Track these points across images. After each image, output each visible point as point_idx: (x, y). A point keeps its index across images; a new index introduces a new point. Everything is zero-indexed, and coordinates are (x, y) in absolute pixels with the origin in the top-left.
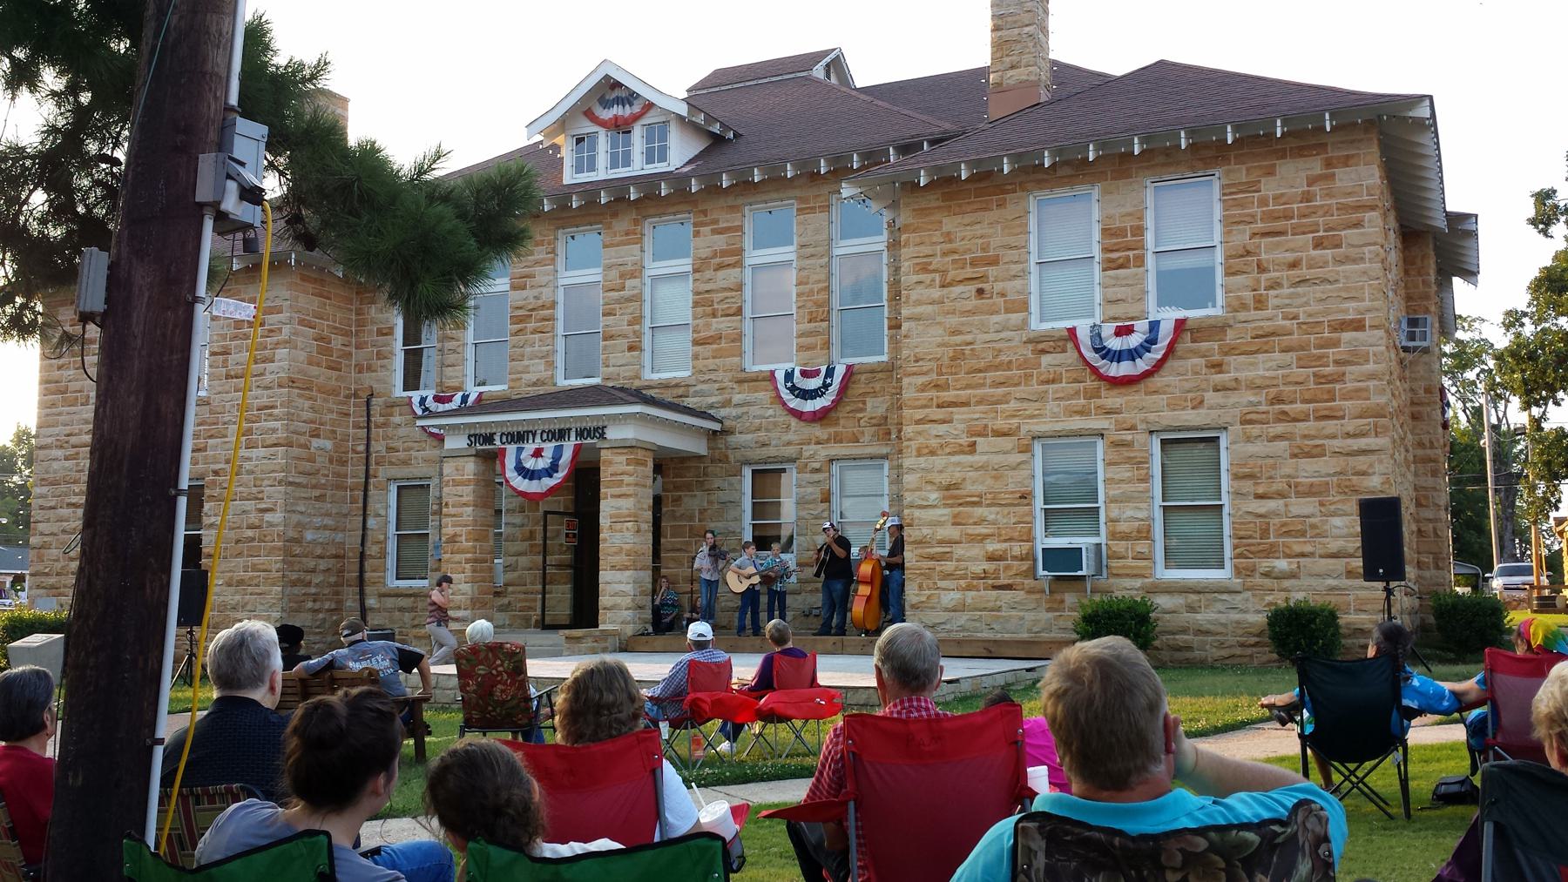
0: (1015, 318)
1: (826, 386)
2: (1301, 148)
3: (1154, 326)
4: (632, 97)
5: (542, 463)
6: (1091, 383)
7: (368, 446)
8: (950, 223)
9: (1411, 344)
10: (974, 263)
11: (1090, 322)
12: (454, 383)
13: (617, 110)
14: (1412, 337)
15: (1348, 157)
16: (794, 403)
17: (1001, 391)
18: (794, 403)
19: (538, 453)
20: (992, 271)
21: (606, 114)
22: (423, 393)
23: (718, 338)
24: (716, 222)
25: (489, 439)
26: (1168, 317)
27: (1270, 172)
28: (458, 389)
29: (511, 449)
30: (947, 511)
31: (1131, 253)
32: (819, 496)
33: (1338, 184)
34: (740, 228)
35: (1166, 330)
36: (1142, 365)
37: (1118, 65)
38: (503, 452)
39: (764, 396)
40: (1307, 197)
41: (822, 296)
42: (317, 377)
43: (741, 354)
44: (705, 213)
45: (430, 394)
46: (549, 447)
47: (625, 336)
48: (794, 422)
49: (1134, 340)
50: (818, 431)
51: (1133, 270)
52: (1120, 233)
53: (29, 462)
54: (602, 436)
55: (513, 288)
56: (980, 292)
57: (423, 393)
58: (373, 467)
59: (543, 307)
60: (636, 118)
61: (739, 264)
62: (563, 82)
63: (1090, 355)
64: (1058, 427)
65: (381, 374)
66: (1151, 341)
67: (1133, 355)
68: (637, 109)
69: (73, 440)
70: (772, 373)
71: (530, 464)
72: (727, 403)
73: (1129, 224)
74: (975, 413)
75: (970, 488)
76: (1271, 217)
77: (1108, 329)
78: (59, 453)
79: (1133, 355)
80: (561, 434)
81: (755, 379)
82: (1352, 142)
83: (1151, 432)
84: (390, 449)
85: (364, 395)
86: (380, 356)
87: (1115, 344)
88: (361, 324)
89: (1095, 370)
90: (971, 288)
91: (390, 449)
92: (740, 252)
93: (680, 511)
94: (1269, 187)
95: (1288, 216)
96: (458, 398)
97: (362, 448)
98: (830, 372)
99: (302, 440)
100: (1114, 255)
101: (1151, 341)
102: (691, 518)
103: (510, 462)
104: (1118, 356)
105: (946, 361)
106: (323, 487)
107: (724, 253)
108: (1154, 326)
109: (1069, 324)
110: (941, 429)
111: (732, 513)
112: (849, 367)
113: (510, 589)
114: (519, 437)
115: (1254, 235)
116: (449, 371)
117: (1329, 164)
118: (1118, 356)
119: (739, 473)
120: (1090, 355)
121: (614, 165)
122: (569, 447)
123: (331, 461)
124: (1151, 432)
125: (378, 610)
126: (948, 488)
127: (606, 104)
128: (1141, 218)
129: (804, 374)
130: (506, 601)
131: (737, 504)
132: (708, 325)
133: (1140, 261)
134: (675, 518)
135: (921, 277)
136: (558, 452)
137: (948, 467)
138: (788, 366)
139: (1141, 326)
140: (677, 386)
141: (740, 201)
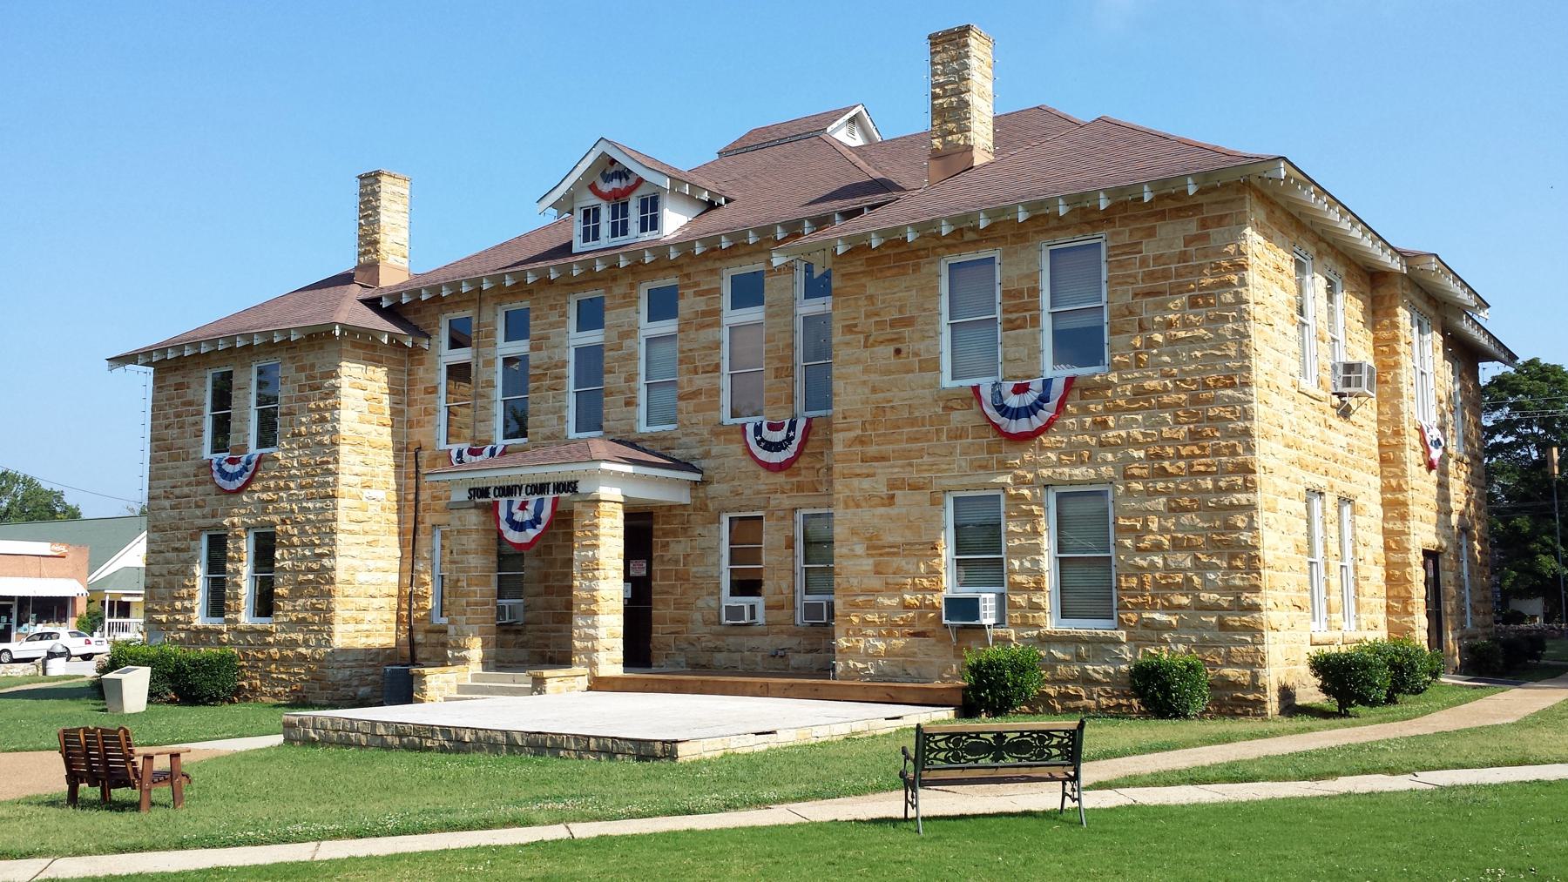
0: (928, 377)
1: (789, 439)
2: (1179, 209)
3: (1047, 384)
4: (624, 174)
5: (526, 516)
6: (991, 436)
7: (417, 494)
8: (872, 287)
9: (1346, 390)
10: (893, 324)
11: (992, 380)
12: (483, 437)
13: (616, 184)
14: (1347, 383)
15: (1221, 218)
16: (764, 455)
17: (914, 446)
18: (764, 455)
19: (523, 507)
20: (906, 331)
21: (606, 188)
22: (461, 446)
23: (696, 394)
24: (697, 284)
25: (484, 492)
26: (1058, 374)
27: (1151, 233)
28: (488, 442)
29: (503, 501)
30: (871, 561)
31: (1027, 314)
32: (783, 543)
33: (1213, 244)
34: (718, 290)
35: (1058, 388)
36: (1037, 422)
37: (1085, 115)
38: (497, 503)
39: (737, 448)
40: (1183, 257)
41: (788, 352)
42: (369, 433)
43: (718, 409)
44: (688, 276)
45: (465, 446)
46: (534, 499)
47: (622, 393)
48: (763, 473)
49: (1029, 398)
50: (781, 478)
51: (1029, 330)
52: (1017, 294)
53: (1236, 331)
54: (574, 490)
55: (532, 349)
56: (898, 352)
57: (461, 446)
58: (421, 514)
59: (556, 366)
60: (630, 190)
61: (718, 324)
62: (569, 161)
63: (990, 412)
64: (966, 481)
65: (428, 428)
66: (1044, 399)
67: (1029, 411)
68: (632, 181)
69: (177, 491)
70: (976, 389)
71: (519, 516)
72: (706, 455)
73: (1025, 285)
74: (896, 470)
75: (889, 539)
76: (1151, 276)
77: (1008, 386)
78: (167, 503)
79: (1029, 411)
80: (540, 489)
81: (729, 430)
82: (1225, 202)
83: (1046, 486)
84: (434, 498)
85: (412, 448)
86: (427, 412)
87: (1013, 401)
88: (411, 383)
89: (996, 427)
90: (891, 349)
91: (434, 498)
92: (717, 312)
93: (668, 555)
94: (1149, 249)
95: (1165, 275)
96: (487, 451)
97: (411, 497)
98: (792, 426)
99: (354, 491)
100: (1014, 316)
101: (1044, 399)
102: (677, 562)
103: (503, 513)
104: (1016, 414)
105: (869, 417)
106: (375, 532)
107: (705, 314)
108: (1047, 384)
109: (973, 382)
110: (866, 484)
111: (712, 559)
112: (809, 420)
113: (529, 627)
114: (508, 491)
115: (1136, 295)
116: (481, 426)
117: (1204, 224)
118: (1016, 414)
119: (718, 520)
120: (990, 412)
121: (614, 234)
122: (548, 498)
123: (383, 509)
124: (1046, 486)
125: (424, 645)
126: (870, 539)
127: (607, 178)
128: (1037, 281)
129: (772, 427)
130: (525, 638)
131: (717, 549)
132: (690, 381)
133: (1035, 321)
134: (663, 562)
135: (848, 337)
136: (540, 502)
137: (872, 516)
138: (757, 419)
139: (1036, 385)
140: (664, 439)
141: (718, 264)
